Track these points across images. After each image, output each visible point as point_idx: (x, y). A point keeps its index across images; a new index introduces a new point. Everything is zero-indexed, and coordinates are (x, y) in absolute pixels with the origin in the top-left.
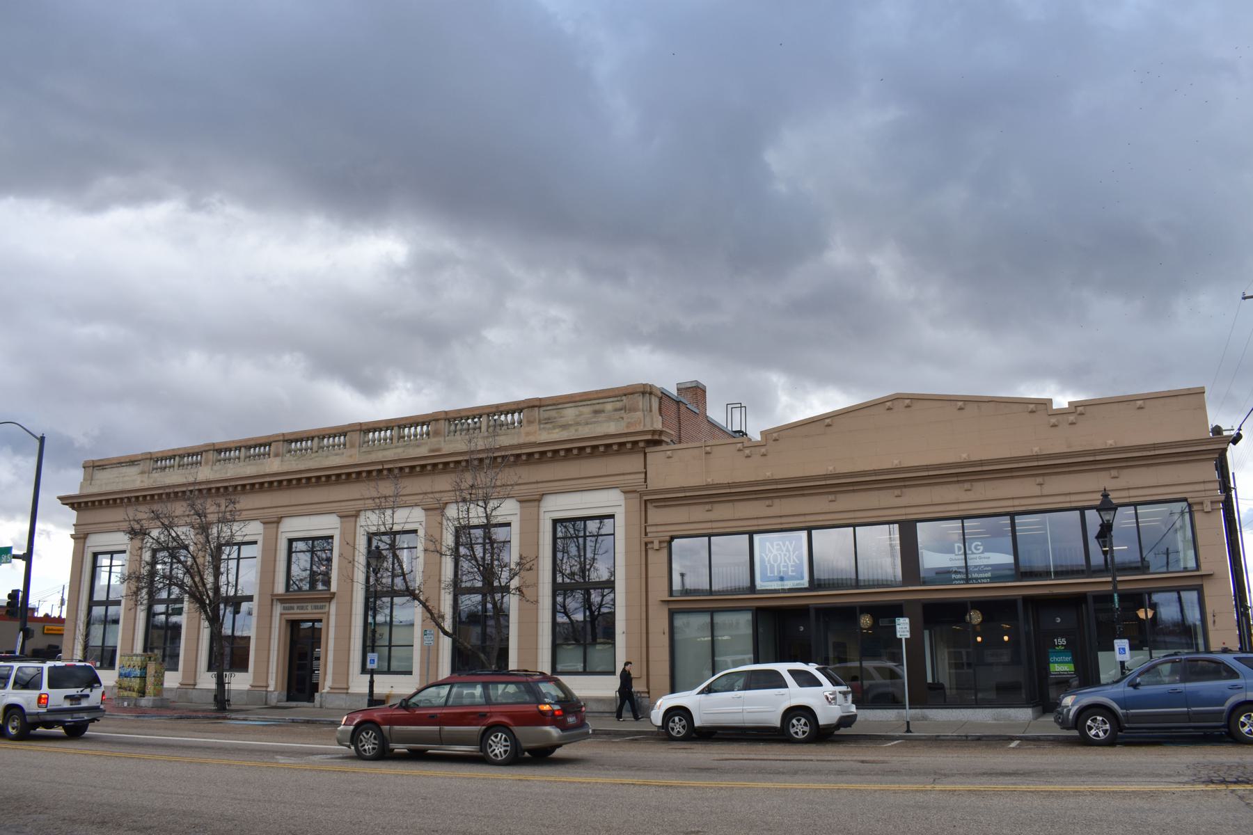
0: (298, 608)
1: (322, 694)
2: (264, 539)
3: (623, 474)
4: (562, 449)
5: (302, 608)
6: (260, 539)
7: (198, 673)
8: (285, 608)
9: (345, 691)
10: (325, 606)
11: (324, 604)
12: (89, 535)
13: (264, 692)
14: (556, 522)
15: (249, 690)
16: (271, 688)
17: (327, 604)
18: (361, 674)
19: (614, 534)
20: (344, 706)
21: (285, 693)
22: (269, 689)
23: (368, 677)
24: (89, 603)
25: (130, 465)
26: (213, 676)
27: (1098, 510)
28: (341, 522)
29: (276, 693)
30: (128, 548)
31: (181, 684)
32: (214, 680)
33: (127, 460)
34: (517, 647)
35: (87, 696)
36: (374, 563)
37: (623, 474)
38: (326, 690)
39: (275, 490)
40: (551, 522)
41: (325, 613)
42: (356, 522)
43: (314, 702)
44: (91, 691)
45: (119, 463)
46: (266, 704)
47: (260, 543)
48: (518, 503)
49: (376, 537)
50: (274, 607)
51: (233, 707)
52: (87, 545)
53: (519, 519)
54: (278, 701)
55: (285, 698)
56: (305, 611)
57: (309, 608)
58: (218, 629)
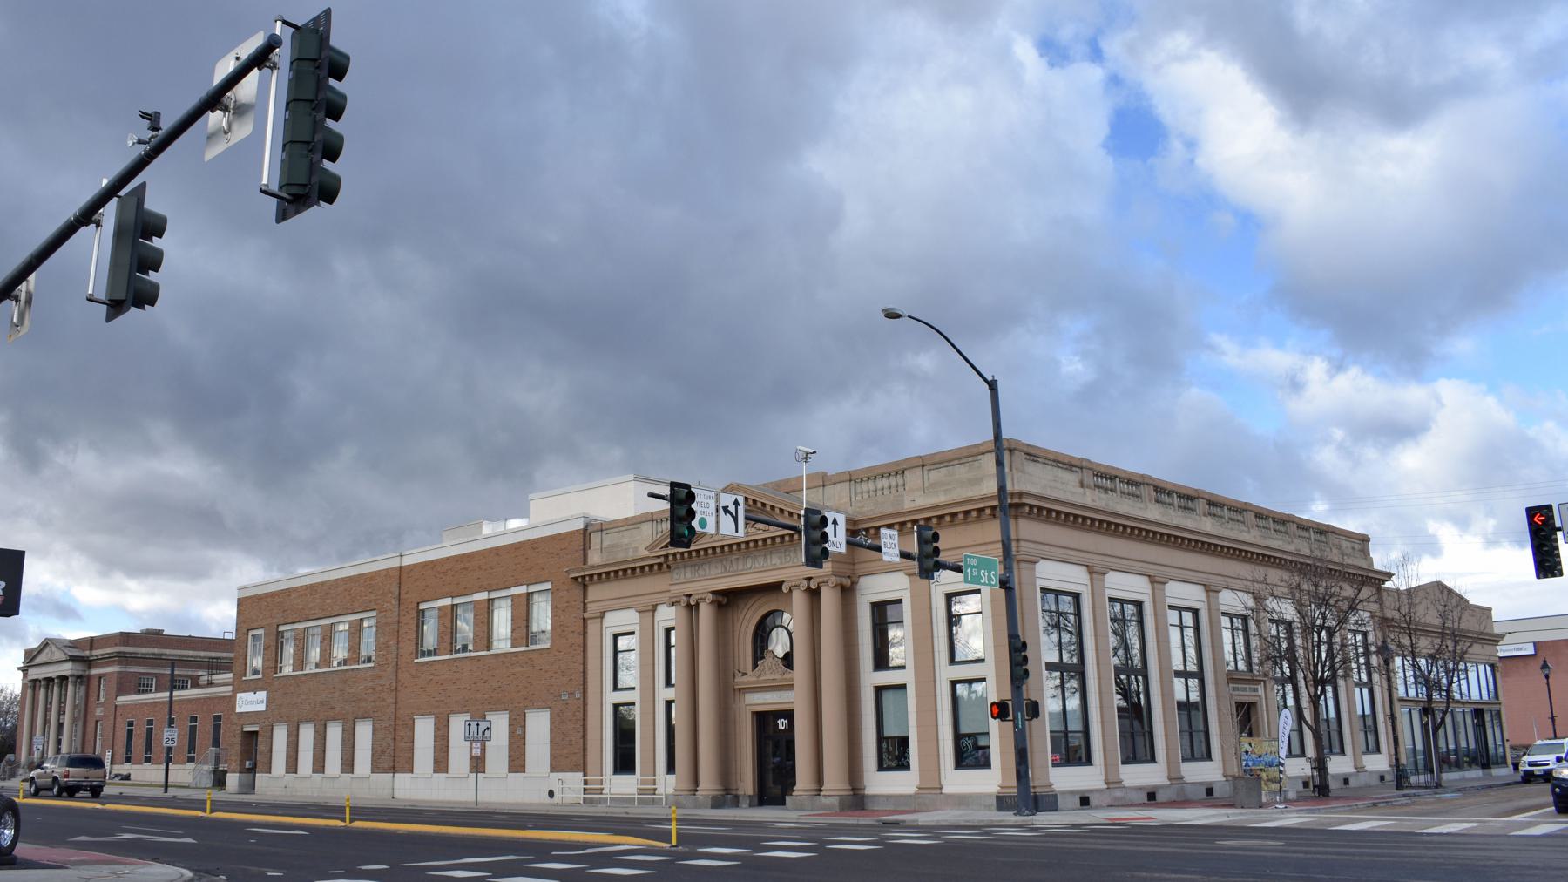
3: (985, 544)
4: (960, 512)
6: (636, 628)
9: (938, 791)
12: (606, 614)
15: (916, 794)
23: (469, 743)
24: (1147, 672)
25: (1066, 469)
28: (911, 582)
30: (636, 628)
31: (1001, 787)
33: (1066, 461)
37: (985, 544)
39: (656, 574)
45: (1054, 461)
47: (637, 633)
48: (907, 577)
52: (657, 619)
57: (670, 693)
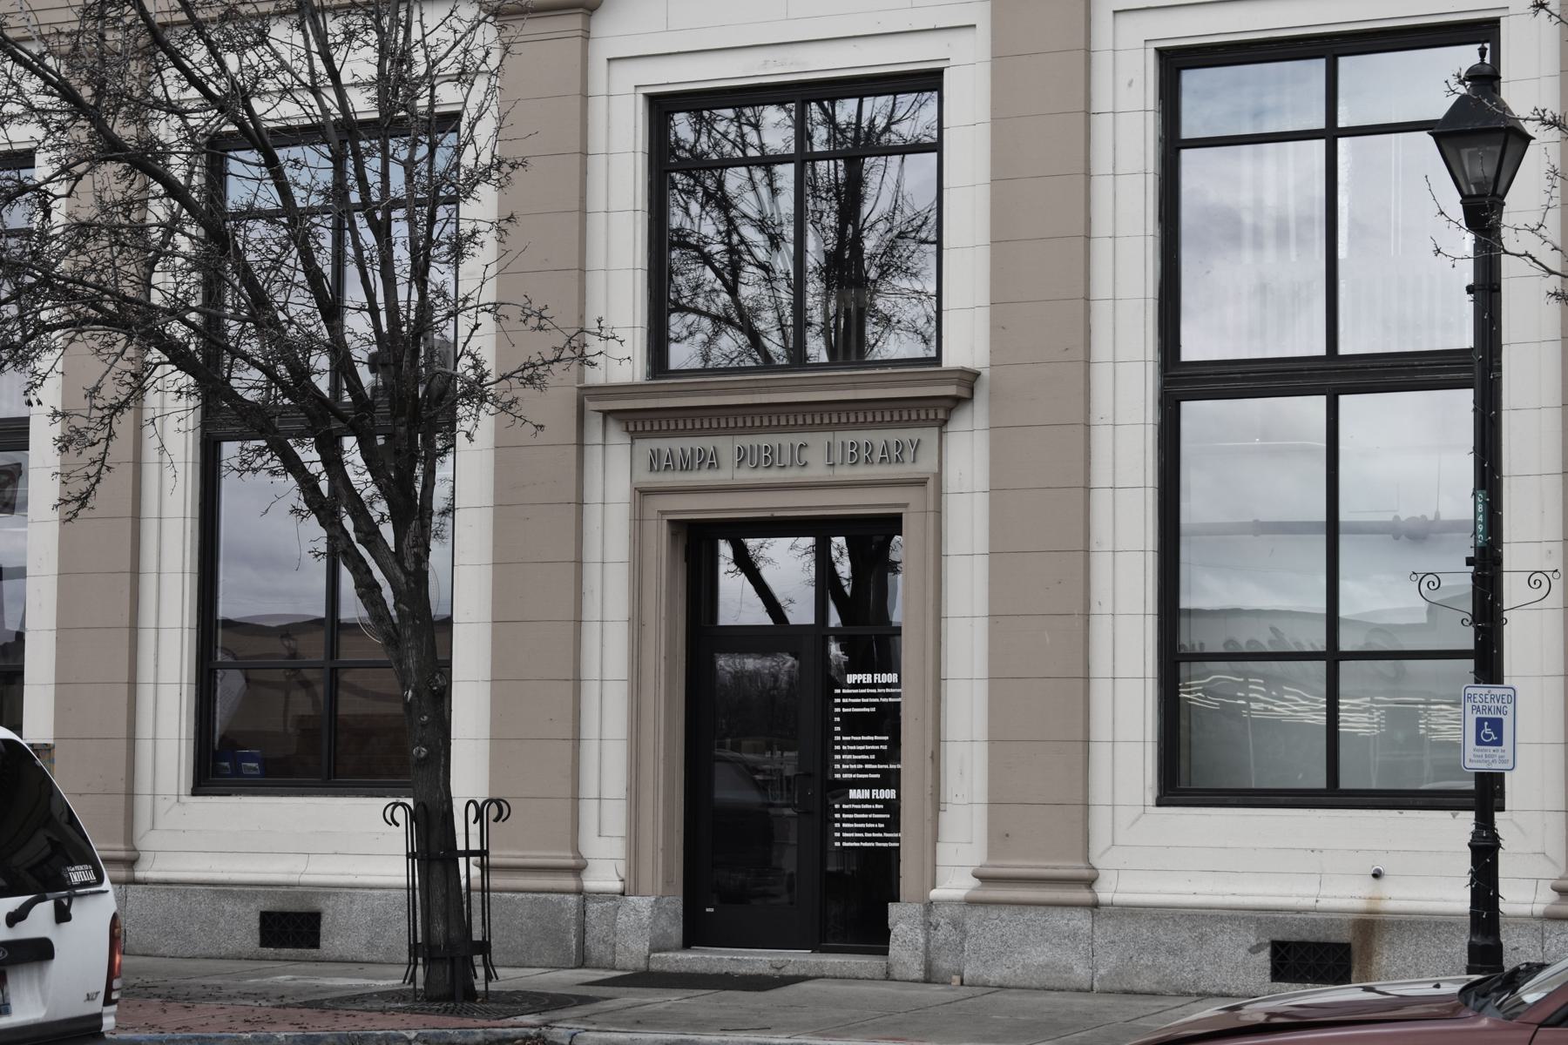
0: (742, 457)
1: (930, 906)
2: (1001, 57)
5: (769, 458)
7: (143, 805)
8: (655, 462)
9: (1082, 895)
10: (917, 446)
11: (905, 435)
13: (572, 899)
14: (661, 106)
16: (604, 875)
17: (929, 435)
18: (1159, 804)
19: (937, 147)
20: (1081, 973)
21: (676, 903)
22: (591, 883)
26: (400, 814)
27: (1438, 138)
29: (642, 904)
32: (397, 839)
34: (487, 674)
35: (41, 951)
36: (819, 226)
38: (954, 884)
40: (641, 103)
41: (921, 483)
42: (586, 36)
43: (885, 952)
44: (62, 915)
46: (583, 962)
49: (241, 154)
50: (594, 455)
51: (509, 978)
53: (986, 54)
54: (653, 950)
55: (676, 932)
56: (792, 475)
58: (410, 565)
